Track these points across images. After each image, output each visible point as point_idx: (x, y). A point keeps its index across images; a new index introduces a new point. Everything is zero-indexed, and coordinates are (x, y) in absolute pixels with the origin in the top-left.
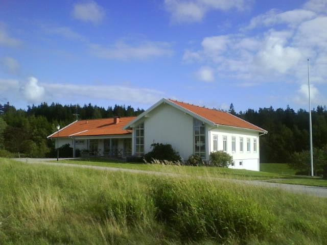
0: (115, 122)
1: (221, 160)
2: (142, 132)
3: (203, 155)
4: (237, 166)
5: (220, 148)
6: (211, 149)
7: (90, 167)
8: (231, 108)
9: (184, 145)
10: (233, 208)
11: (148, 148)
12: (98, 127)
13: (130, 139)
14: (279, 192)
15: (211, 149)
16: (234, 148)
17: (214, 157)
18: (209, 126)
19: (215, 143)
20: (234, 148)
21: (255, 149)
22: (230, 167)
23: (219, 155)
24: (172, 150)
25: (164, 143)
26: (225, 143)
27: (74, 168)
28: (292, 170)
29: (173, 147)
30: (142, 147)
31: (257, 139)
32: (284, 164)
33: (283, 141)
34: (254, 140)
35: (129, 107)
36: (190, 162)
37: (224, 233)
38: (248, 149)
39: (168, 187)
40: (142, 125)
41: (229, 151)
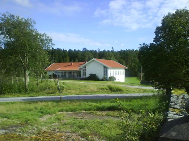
0: (72, 65)
1: (112, 79)
2: (85, 69)
3: (107, 78)
4: (117, 81)
5: (112, 75)
6: (109, 76)
7: (84, 83)
8: (112, 49)
9: (101, 75)
10: (119, 88)
11: (88, 75)
12: (66, 66)
13: (81, 72)
14: (126, 87)
15: (109, 76)
16: (116, 75)
17: (110, 78)
18: (109, 68)
19: (110, 73)
20: (116, 75)
21: (123, 74)
22: (115, 81)
23: (112, 78)
24: (93, 74)
25: (93, 74)
26: (113, 73)
27: (62, 82)
28: (138, 81)
29: (97, 75)
30: (85, 75)
31: (124, 70)
32: (135, 78)
33: (137, 67)
34: (123, 71)
35: (58, 48)
36: (102, 80)
37: (118, 91)
38: (121, 74)
39: (110, 86)
40: (85, 67)
41: (115, 76)
